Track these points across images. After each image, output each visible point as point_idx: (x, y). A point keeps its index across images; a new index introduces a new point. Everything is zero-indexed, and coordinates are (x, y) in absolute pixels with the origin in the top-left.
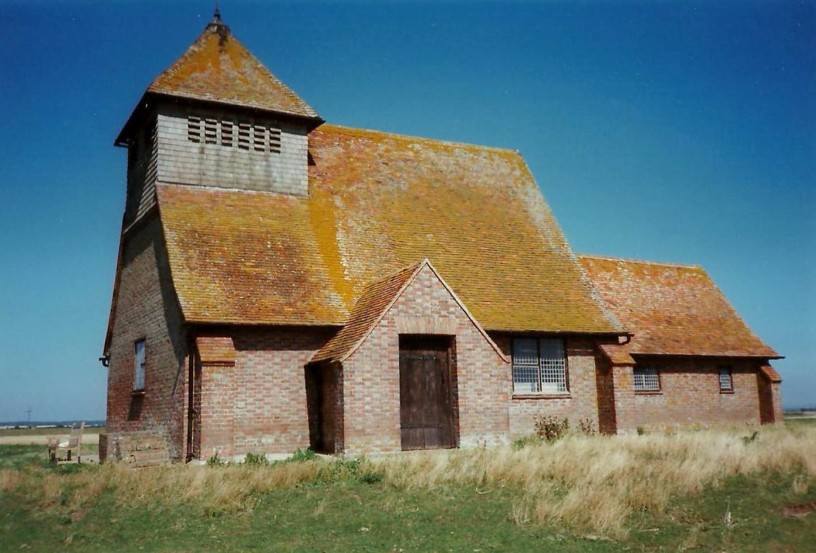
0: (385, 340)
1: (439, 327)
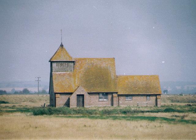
0: (75, 95)
1: (82, 93)
